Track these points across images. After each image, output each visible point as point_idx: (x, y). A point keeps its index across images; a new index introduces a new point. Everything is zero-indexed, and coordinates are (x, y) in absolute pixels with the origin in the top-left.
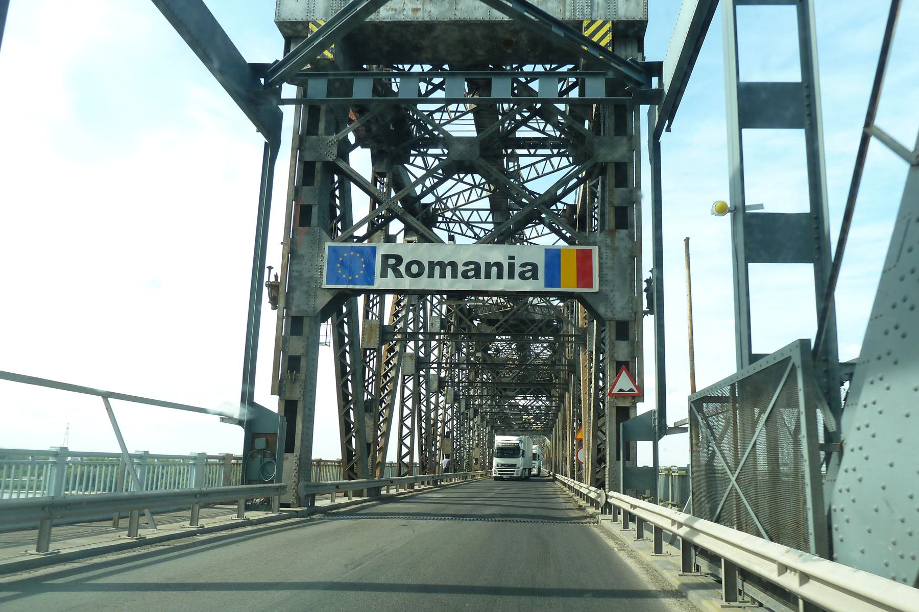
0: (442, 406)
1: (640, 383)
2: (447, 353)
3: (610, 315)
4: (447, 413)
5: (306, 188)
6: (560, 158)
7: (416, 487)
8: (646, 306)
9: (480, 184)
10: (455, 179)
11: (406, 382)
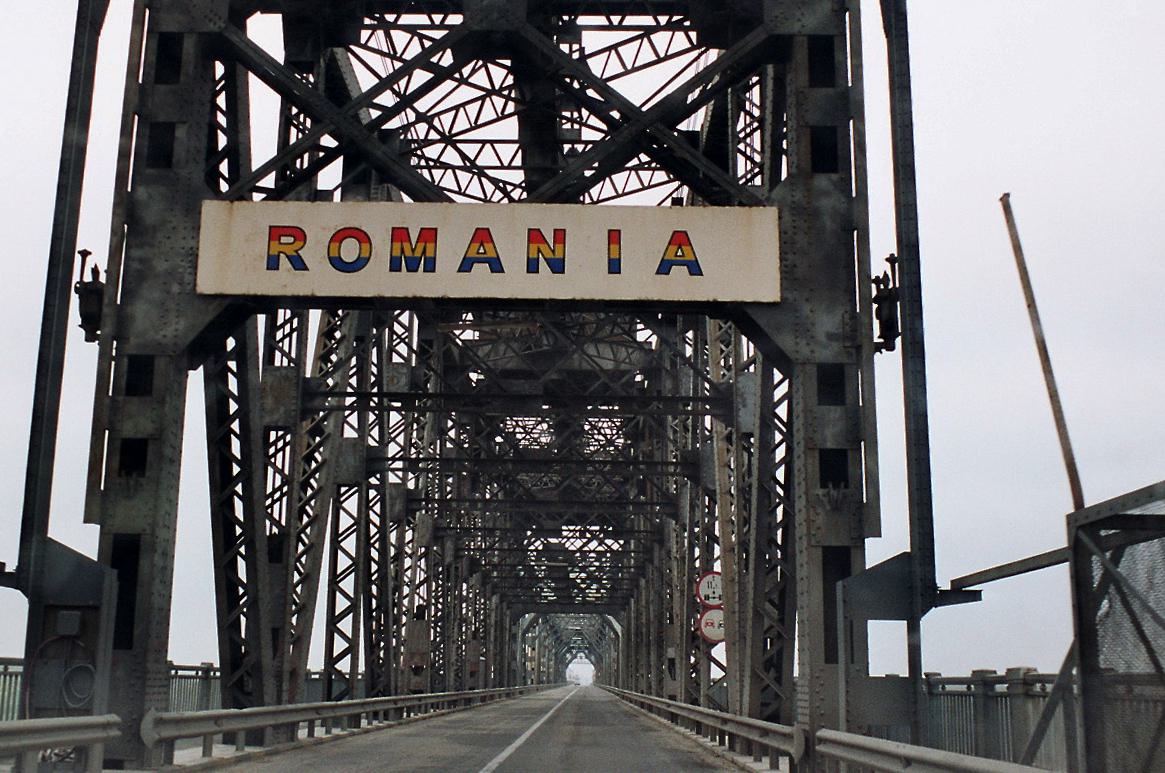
0: (409, 552)
1: (870, 496)
2: (421, 439)
3: (805, 351)
4: (419, 567)
5: (162, 88)
6: (671, 33)
7: (364, 723)
8: (878, 334)
9: (502, 89)
10: (455, 80)
11: (342, 499)
